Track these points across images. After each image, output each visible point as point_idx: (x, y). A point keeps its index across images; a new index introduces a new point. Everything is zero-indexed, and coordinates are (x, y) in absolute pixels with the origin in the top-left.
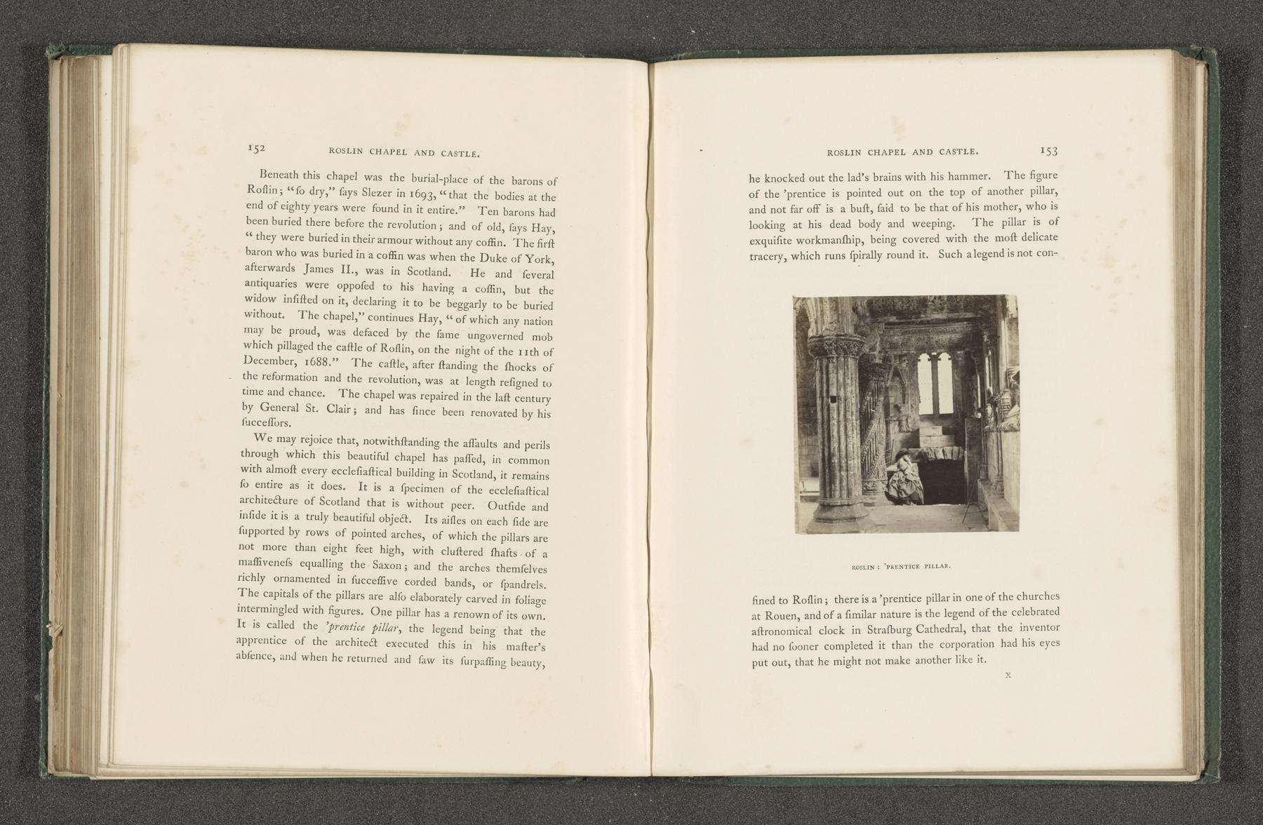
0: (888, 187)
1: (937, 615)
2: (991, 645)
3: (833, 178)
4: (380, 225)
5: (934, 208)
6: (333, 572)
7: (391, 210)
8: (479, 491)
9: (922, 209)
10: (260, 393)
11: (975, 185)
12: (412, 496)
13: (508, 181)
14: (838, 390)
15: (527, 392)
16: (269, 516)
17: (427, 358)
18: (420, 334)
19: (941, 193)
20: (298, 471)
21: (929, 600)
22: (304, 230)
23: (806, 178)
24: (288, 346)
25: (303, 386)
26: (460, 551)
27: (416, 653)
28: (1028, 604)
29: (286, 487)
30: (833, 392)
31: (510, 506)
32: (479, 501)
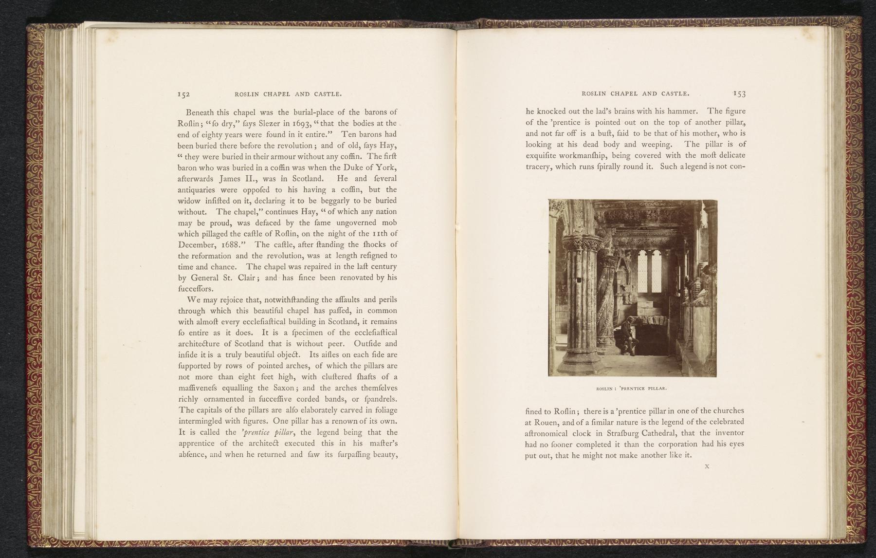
0: (624, 118)
1: (657, 423)
2: (695, 445)
3: (586, 111)
4: (273, 147)
5: (658, 133)
6: (246, 394)
7: (279, 135)
8: (348, 333)
9: (649, 134)
10: (191, 268)
11: (687, 117)
12: (300, 338)
13: (362, 112)
14: (583, 273)
15: (379, 262)
16: (199, 355)
17: (308, 240)
18: (303, 223)
19: (662, 123)
20: (219, 322)
21: (651, 412)
22: (218, 152)
23: (567, 111)
24: (209, 234)
25: (220, 262)
26: (335, 377)
27: (306, 450)
28: (721, 416)
29: (211, 334)
30: (579, 276)
31: (370, 344)
32: (348, 340)
